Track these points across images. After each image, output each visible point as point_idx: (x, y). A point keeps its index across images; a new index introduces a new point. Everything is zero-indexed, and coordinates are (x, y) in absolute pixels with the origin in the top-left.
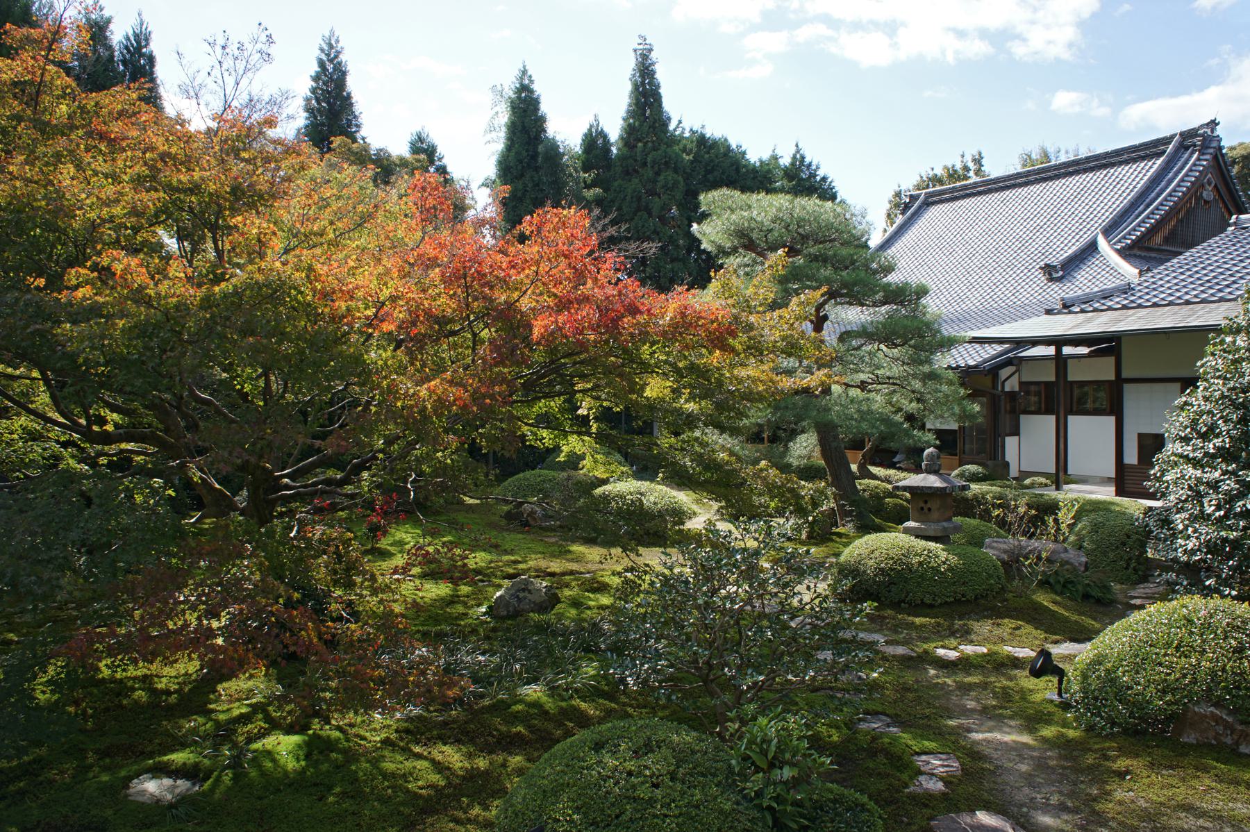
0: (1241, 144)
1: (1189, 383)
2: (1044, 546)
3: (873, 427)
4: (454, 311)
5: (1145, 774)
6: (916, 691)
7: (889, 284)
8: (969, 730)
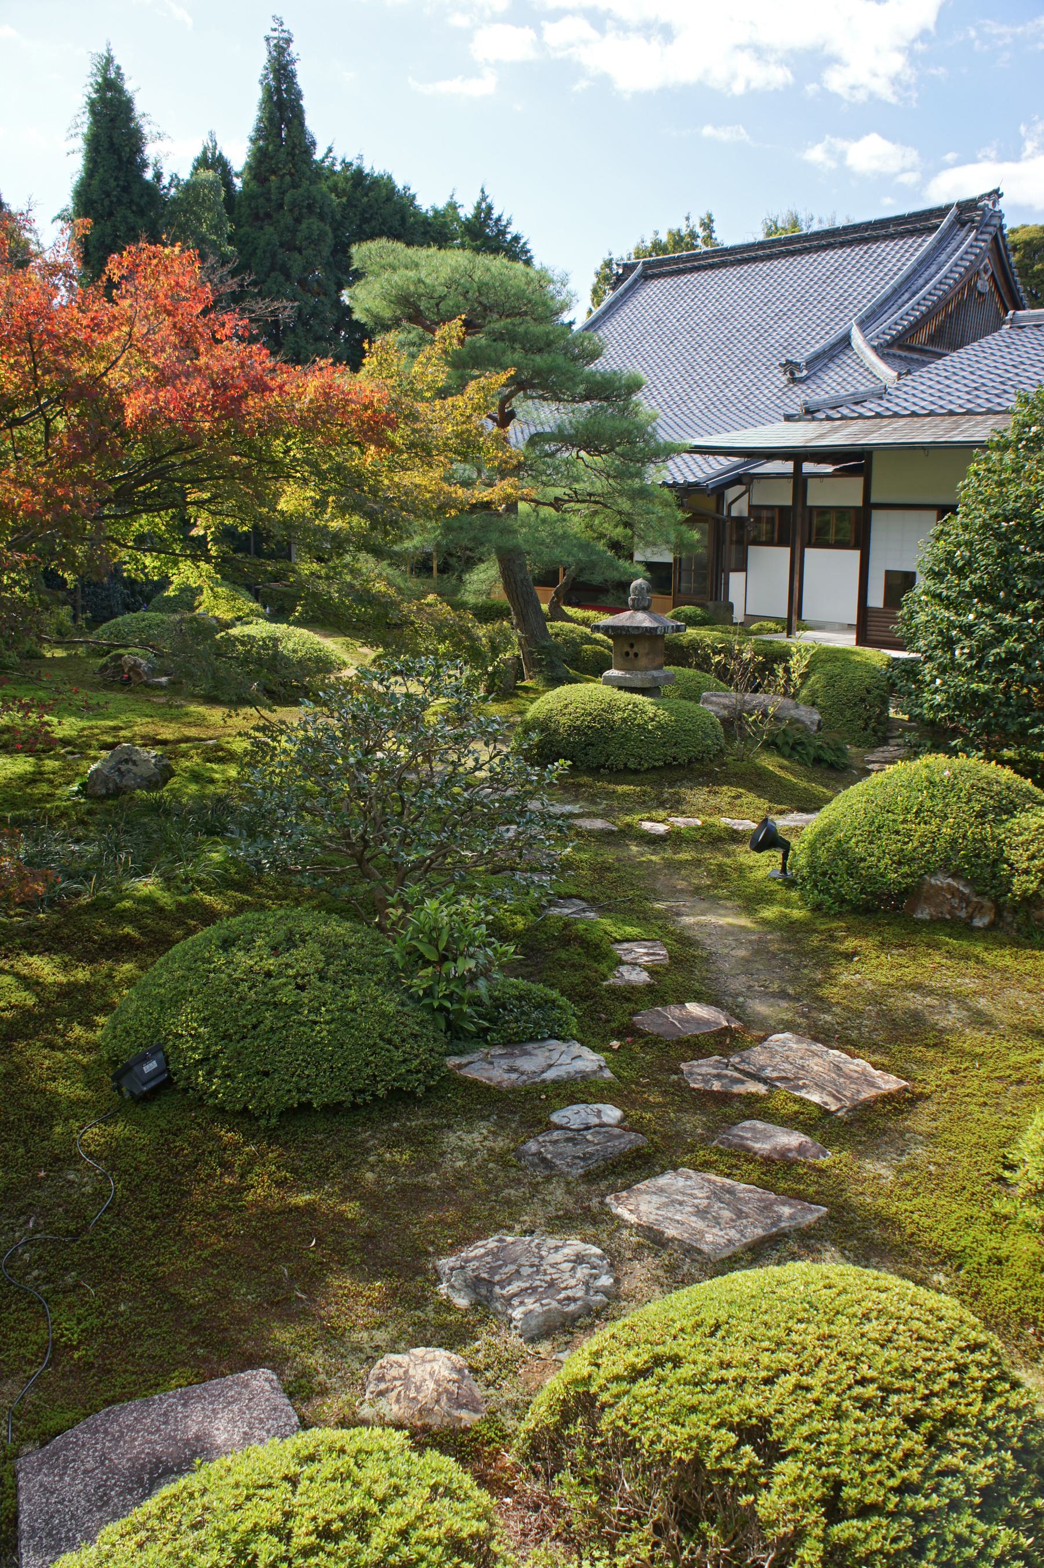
0: (1024, 227)
1: (946, 510)
2: (771, 701)
3: (569, 554)
4: (17, 387)
5: (874, 954)
6: (617, 870)
7: (593, 374)
8: (678, 914)
